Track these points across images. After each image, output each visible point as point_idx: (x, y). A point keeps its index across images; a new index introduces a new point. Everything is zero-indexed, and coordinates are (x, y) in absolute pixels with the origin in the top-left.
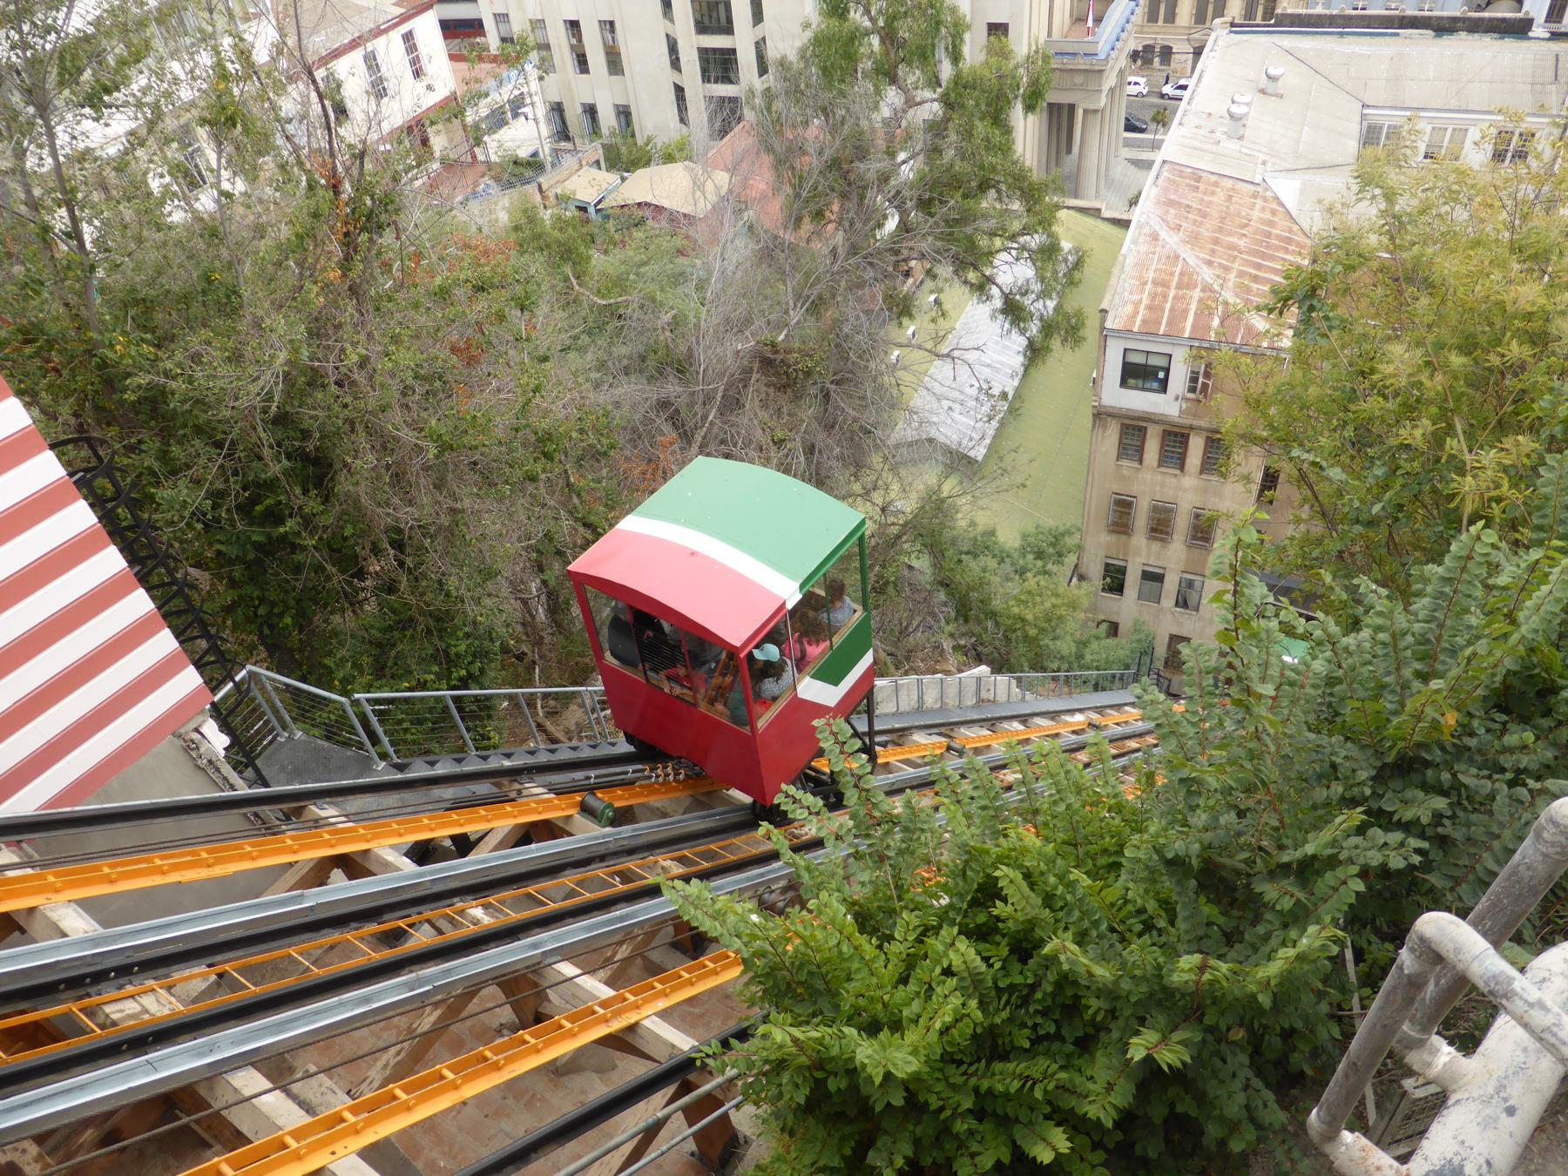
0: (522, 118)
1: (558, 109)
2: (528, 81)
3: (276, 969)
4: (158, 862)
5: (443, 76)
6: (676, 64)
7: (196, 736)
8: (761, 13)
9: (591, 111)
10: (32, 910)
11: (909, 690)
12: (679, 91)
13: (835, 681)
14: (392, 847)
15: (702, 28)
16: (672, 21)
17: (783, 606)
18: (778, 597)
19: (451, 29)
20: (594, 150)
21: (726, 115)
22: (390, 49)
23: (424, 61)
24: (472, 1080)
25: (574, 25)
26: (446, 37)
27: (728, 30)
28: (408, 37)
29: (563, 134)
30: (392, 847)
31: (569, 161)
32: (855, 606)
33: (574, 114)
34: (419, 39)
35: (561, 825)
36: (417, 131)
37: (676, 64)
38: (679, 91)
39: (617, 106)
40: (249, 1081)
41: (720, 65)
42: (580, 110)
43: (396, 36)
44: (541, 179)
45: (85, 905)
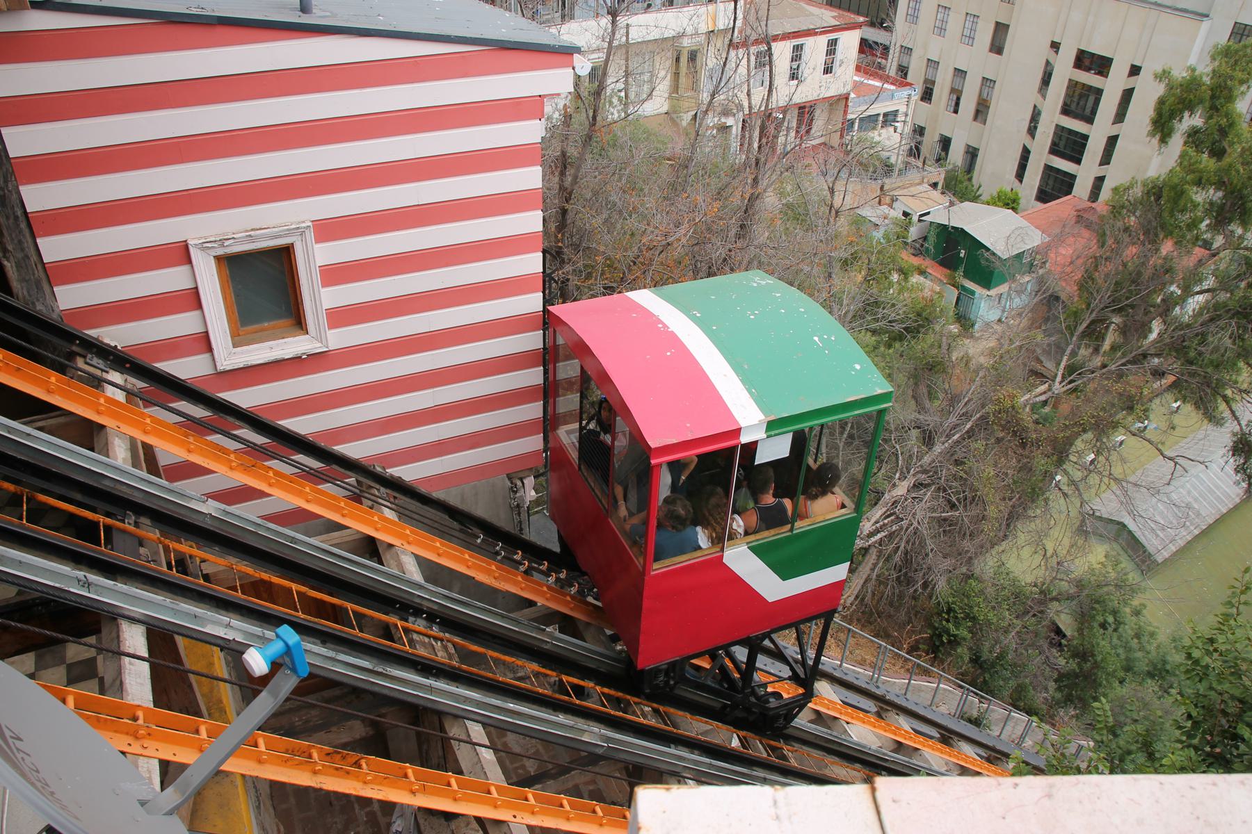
0: (892, 129)
1: (920, 131)
2: (901, 101)
3: (478, 659)
4: (467, 556)
5: (846, 76)
6: (1032, 131)
7: (519, 483)
8: (1124, 115)
9: (946, 143)
10: (391, 546)
11: (1016, 724)
12: (1026, 154)
13: (785, 570)
14: (417, 557)
15: (1066, 111)
16: (1044, 97)
17: (737, 432)
18: (736, 422)
19: (866, 46)
20: (938, 174)
21: (1056, 186)
22: (815, 48)
23: (836, 63)
24: (582, 820)
25: (960, 73)
26: (861, 51)
27: (1090, 120)
28: (833, 44)
29: (915, 151)
30: (417, 557)
31: (913, 175)
32: (848, 502)
33: (930, 143)
34: (840, 47)
35: (581, 628)
36: (805, 112)
37: (1032, 131)
38: (1026, 154)
39: (968, 146)
40: (477, 732)
41: (1070, 145)
42: (937, 138)
43: (822, 41)
44: (887, 181)
45: (421, 561)
